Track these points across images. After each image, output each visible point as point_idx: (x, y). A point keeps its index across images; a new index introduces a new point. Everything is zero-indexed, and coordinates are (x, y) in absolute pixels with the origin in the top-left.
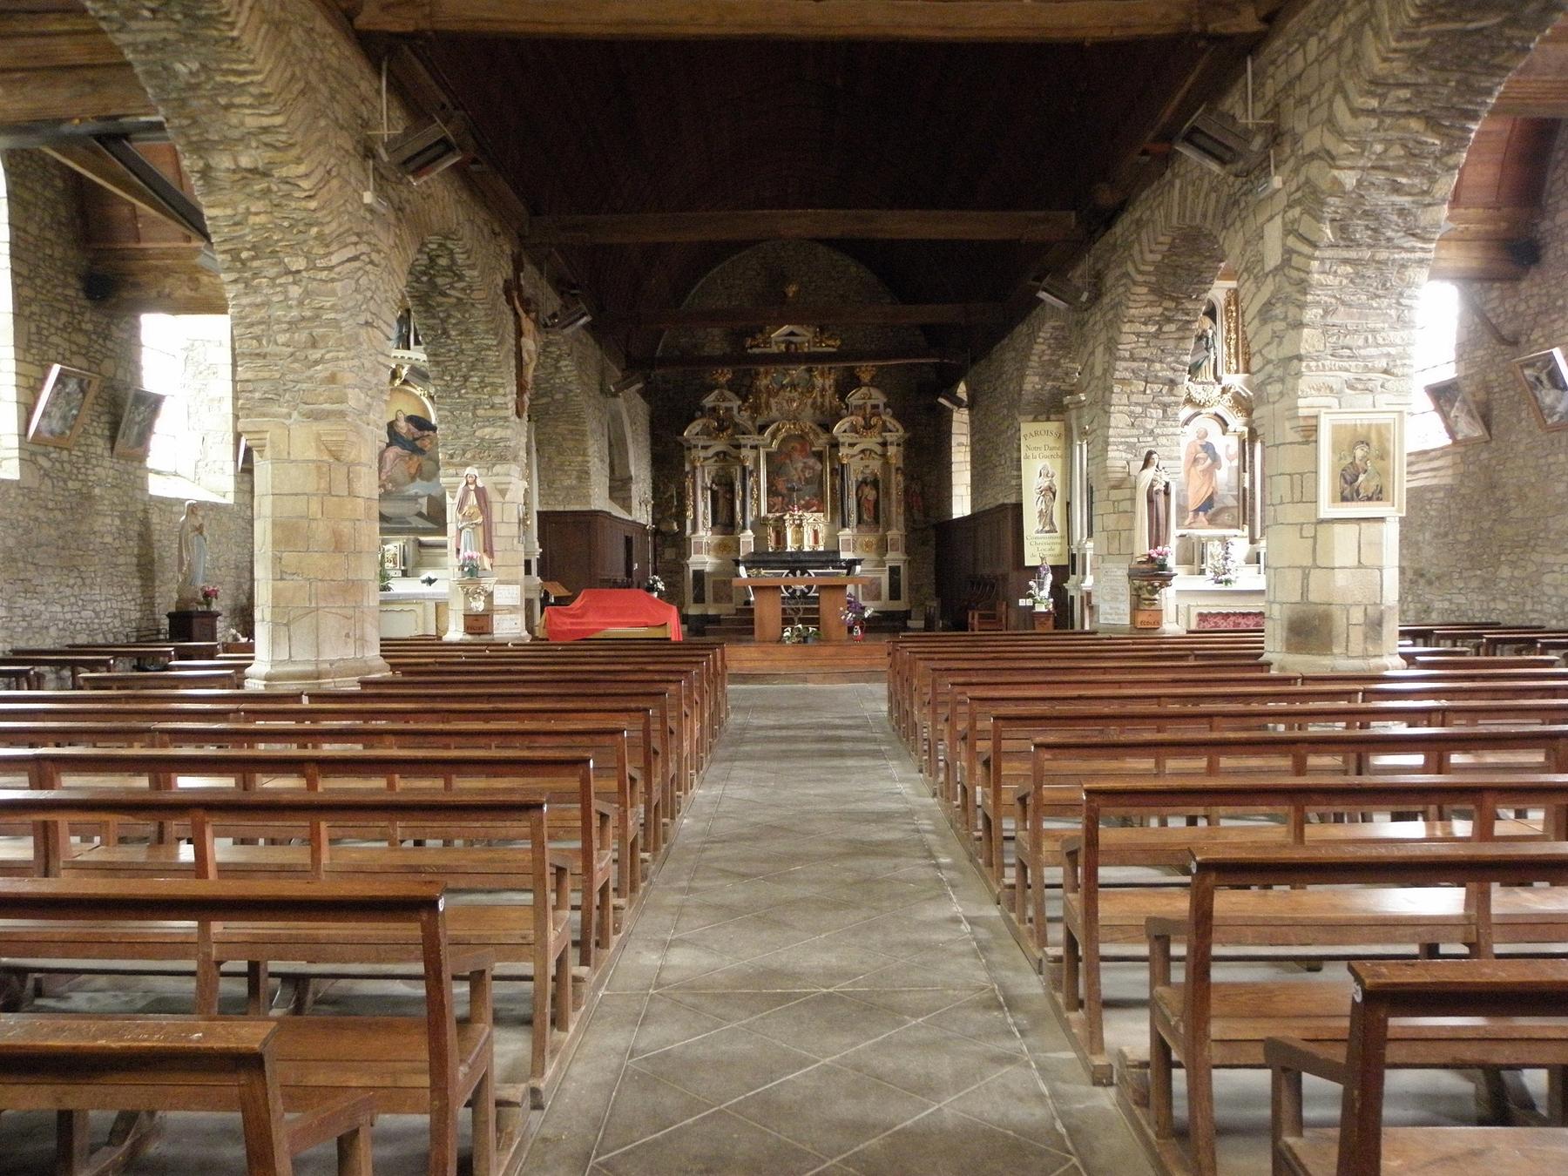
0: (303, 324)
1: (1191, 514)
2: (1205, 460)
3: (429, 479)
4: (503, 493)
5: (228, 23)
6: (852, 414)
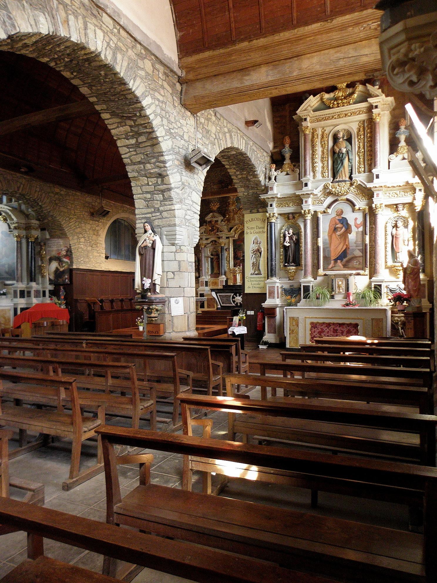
1: (332, 262)
2: (341, 228)
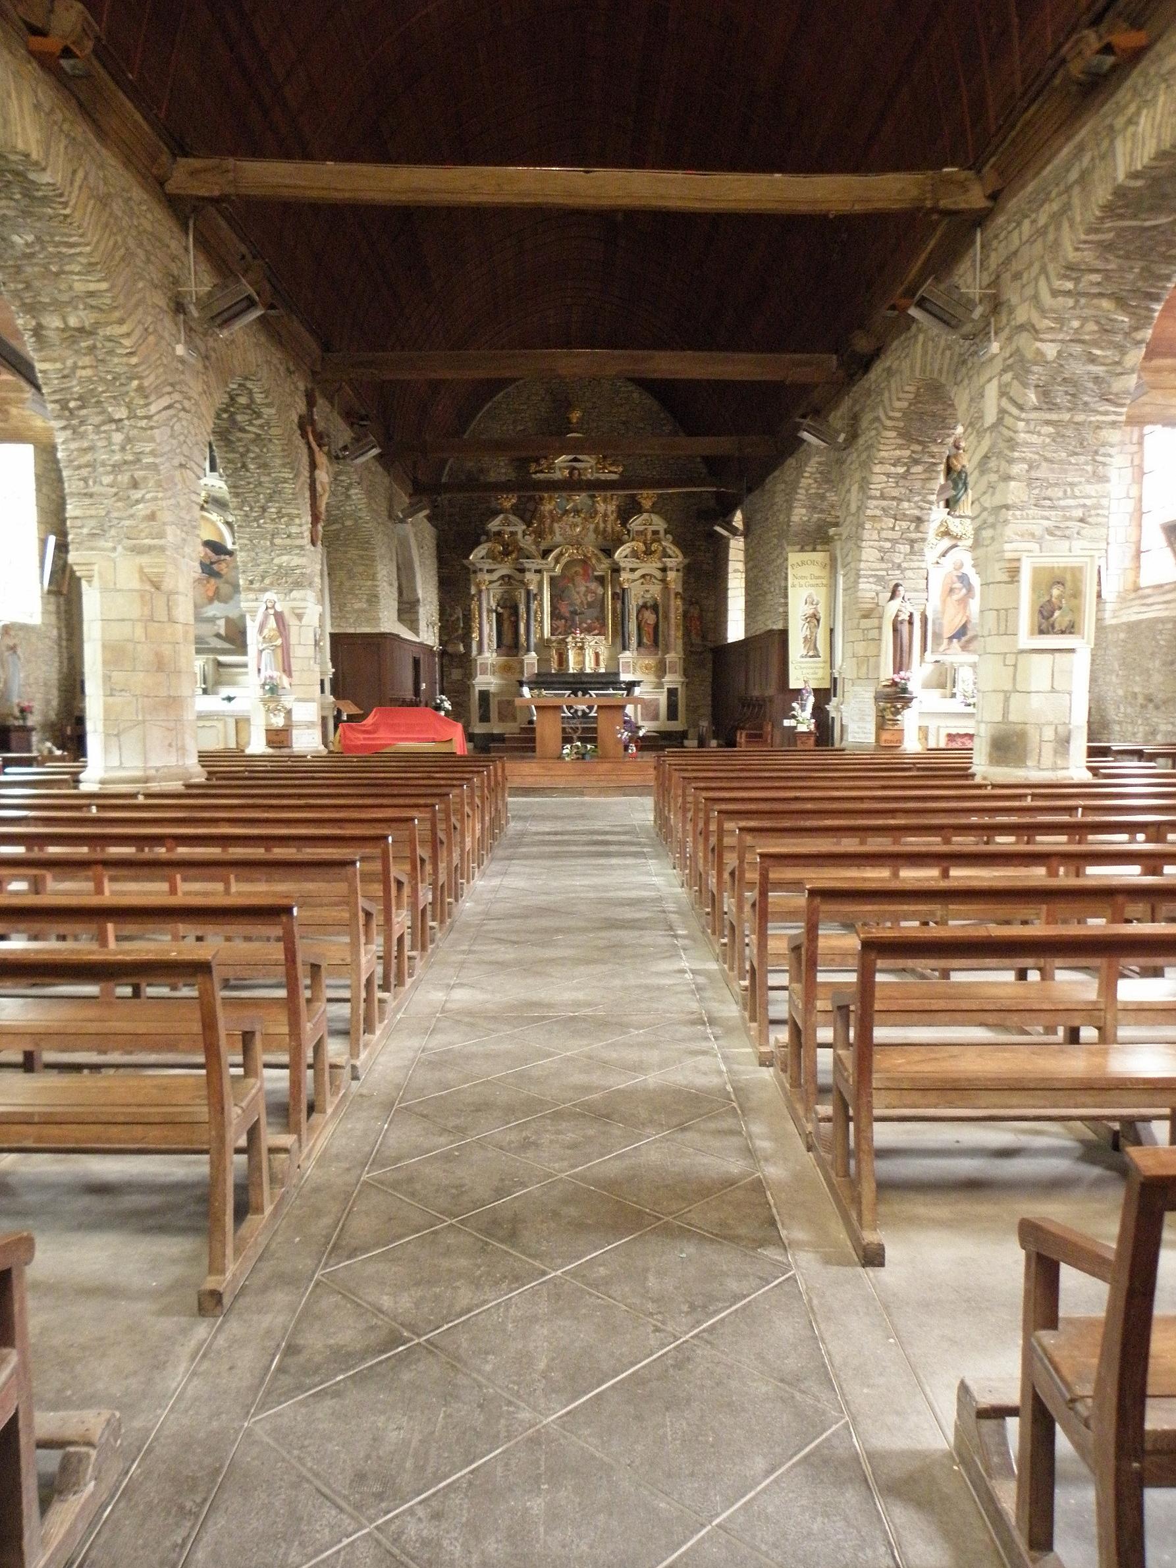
0: (126, 467)
1: (946, 641)
2: (960, 589)
3: (225, 601)
4: (299, 617)
5: (60, 203)
6: (633, 540)
